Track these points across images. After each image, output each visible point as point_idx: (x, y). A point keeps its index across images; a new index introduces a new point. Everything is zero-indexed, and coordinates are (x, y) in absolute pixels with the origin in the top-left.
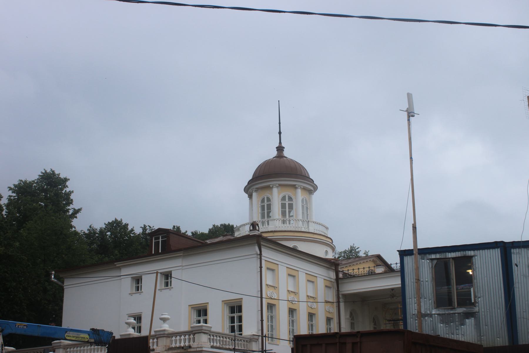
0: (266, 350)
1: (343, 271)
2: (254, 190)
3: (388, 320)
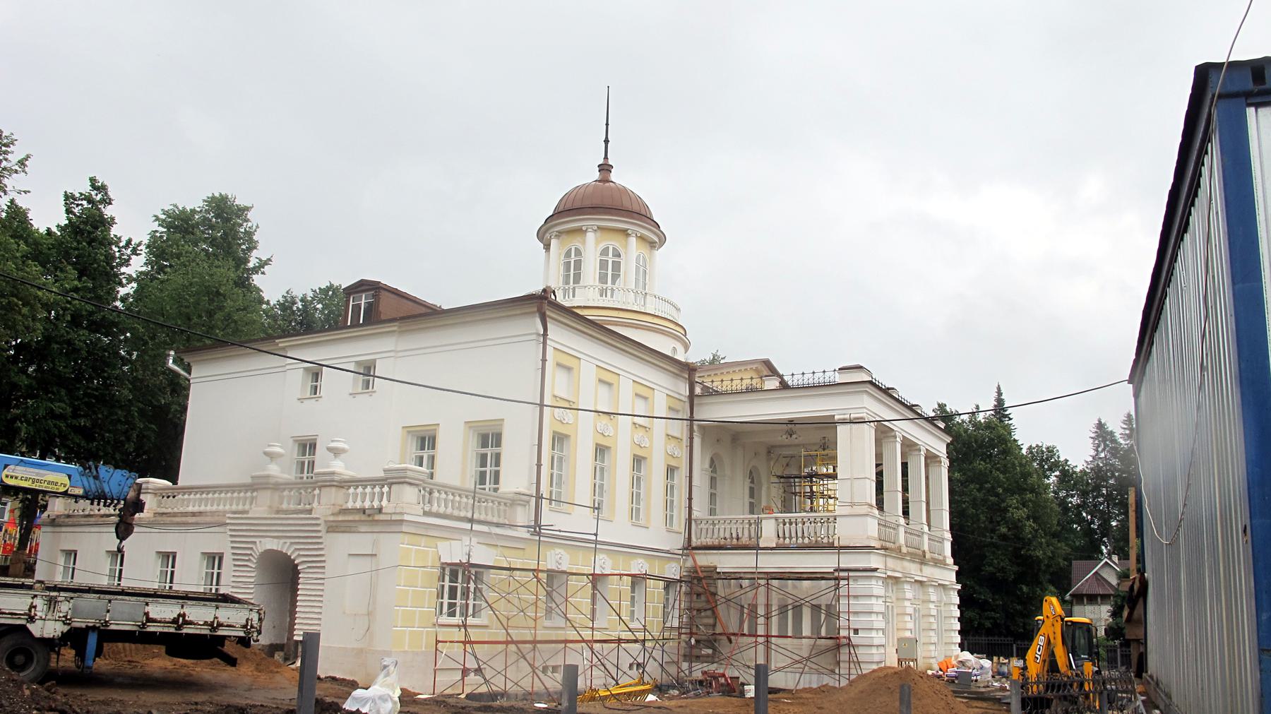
0: (542, 524)
1: (703, 382)
3: (778, 477)
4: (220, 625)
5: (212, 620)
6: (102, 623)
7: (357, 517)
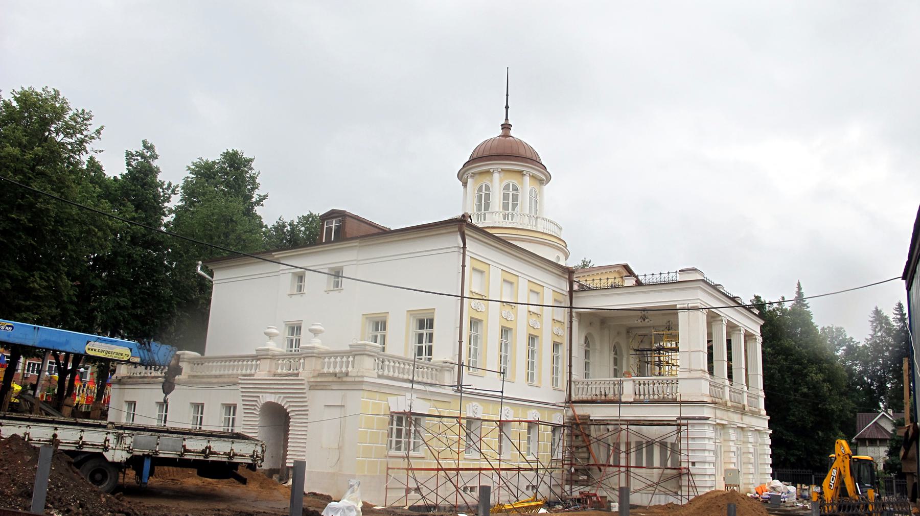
1: (579, 281)
3: (635, 350)
4: (235, 455)
5: (229, 451)
7: (330, 379)
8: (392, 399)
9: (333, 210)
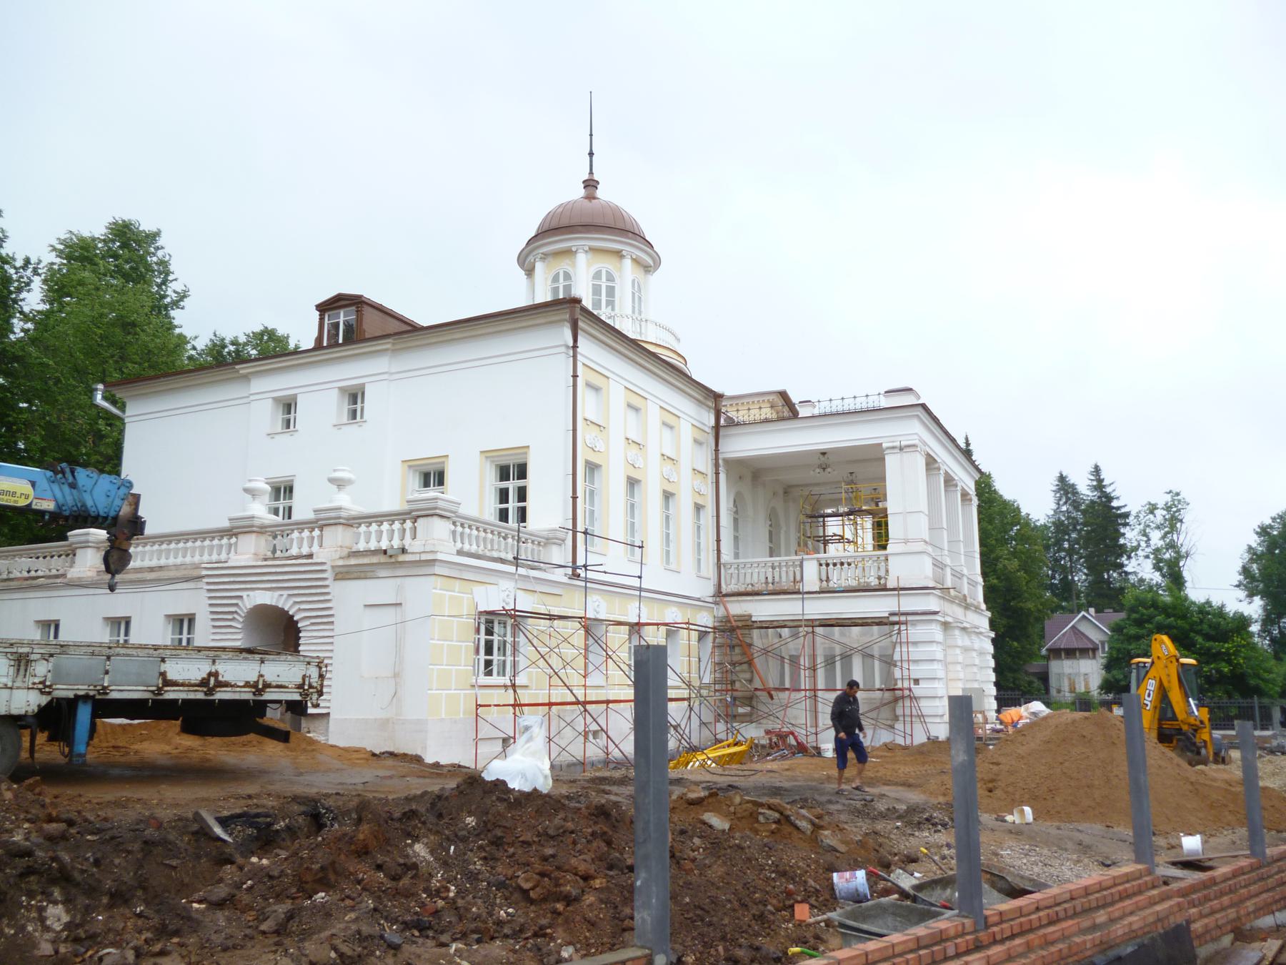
2: (540, 255)
4: (267, 685)
5: (256, 679)
6: (98, 690)
7: (375, 560)
8: (479, 591)
9: (339, 295)
